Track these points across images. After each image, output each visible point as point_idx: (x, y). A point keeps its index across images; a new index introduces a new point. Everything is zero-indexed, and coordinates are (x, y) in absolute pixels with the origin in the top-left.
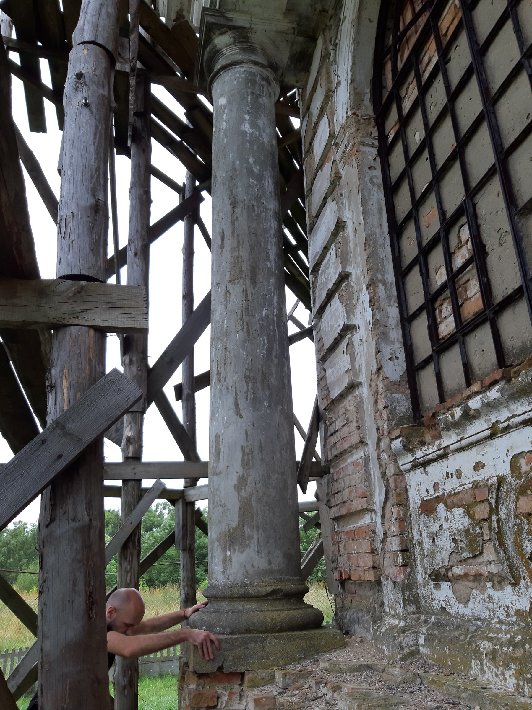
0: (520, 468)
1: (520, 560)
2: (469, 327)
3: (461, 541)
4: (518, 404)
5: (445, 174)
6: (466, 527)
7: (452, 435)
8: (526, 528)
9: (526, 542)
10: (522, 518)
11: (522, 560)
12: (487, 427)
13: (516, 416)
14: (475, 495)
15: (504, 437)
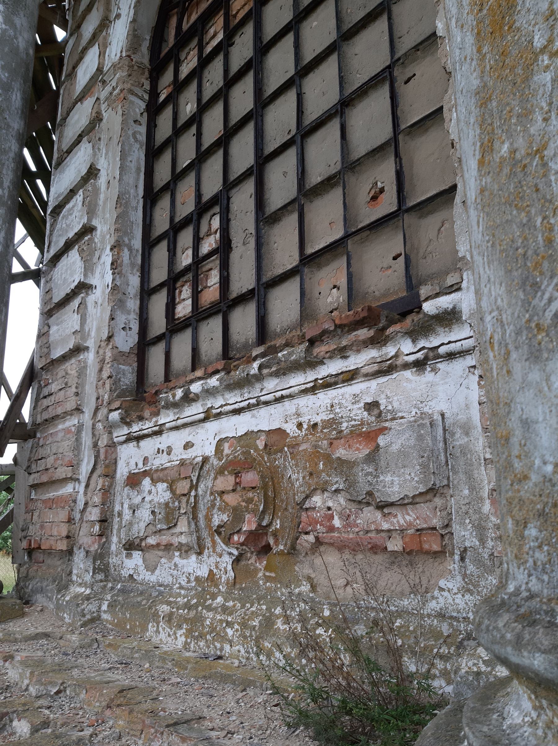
3: (160, 513)
4: (232, 394)
9: (216, 516)
13: (229, 404)
15: (215, 422)
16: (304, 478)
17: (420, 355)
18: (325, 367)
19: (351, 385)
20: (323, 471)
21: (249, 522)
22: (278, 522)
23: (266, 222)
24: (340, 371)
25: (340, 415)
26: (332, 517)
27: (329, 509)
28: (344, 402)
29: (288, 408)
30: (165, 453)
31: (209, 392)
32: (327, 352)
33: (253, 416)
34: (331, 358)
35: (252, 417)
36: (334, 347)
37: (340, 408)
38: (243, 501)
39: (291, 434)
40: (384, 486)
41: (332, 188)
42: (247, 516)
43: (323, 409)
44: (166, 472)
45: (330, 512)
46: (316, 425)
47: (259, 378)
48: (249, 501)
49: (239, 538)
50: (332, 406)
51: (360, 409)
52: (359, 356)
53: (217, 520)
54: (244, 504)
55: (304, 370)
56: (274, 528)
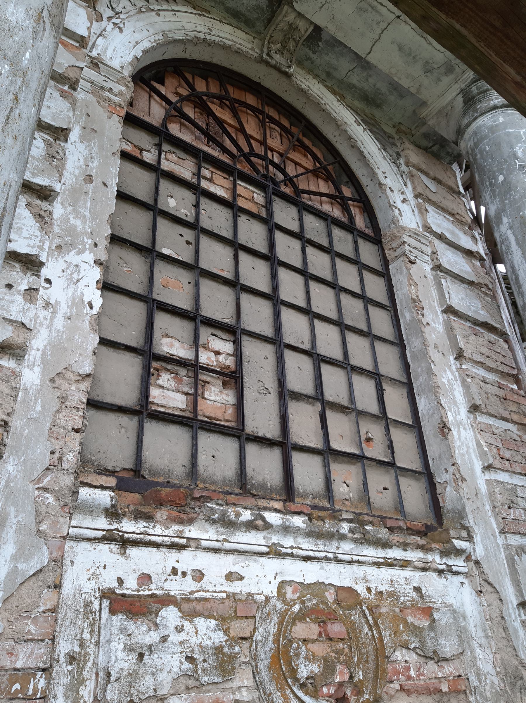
0: (285, 594)
1: (274, 686)
2: (214, 427)
3: (205, 661)
4: (306, 540)
5: (207, 278)
6: (218, 644)
7: (210, 530)
8: (303, 653)
9: (303, 667)
10: (300, 643)
11: (277, 686)
12: (264, 544)
13: (301, 549)
14: (236, 608)
15: (275, 560)
16: (390, 635)
17: (444, 567)
18: (391, 551)
19: (403, 570)
20: (404, 632)
21: (341, 673)
22: (361, 673)
23: (290, 394)
24: (402, 559)
25: (398, 590)
26: (409, 669)
27: (406, 662)
28: (399, 580)
29: (357, 572)
30: (189, 577)
31: (286, 529)
32: (398, 542)
33: (322, 568)
34: (398, 546)
35: (321, 569)
36: (402, 540)
37: (398, 584)
38: (333, 651)
39: (362, 595)
40: (442, 647)
41: (341, 412)
42: (338, 667)
43: (385, 582)
44: (208, 605)
45: (408, 665)
46: (381, 592)
47: (342, 537)
48: (339, 652)
49: (329, 690)
50: (392, 581)
51: (410, 589)
52: (413, 553)
53: (305, 671)
54: (334, 655)
55: (377, 547)
56: (357, 679)
